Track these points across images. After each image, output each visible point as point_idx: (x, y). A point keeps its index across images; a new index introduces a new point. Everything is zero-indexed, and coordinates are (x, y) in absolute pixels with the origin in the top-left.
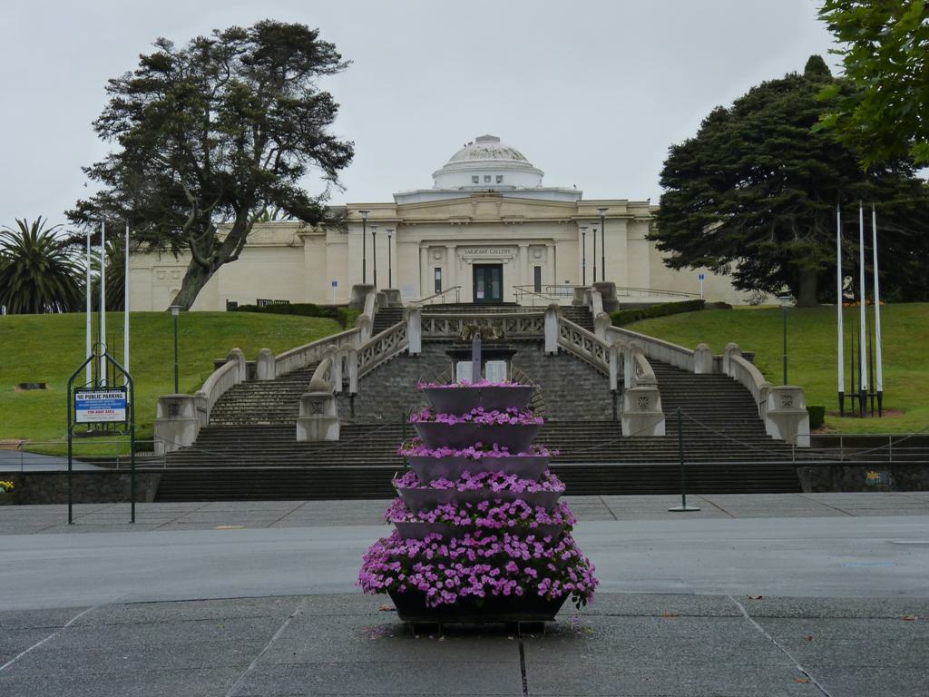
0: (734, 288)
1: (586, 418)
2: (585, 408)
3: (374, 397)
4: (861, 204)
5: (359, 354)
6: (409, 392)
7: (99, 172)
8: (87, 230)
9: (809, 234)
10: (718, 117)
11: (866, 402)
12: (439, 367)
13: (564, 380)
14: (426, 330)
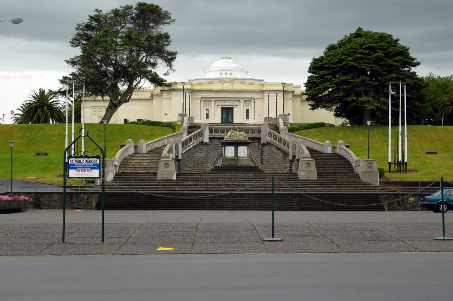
0: (334, 116)
1: (278, 171)
2: (278, 167)
3: (188, 161)
4: (390, 84)
5: (183, 144)
6: (203, 159)
7: (73, 63)
8: (66, 87)
9: (369, 96)
10: (332, 48)
11: (401, 166)
12: (216, 149)
13: (269, 155)
14: (211, 133)
